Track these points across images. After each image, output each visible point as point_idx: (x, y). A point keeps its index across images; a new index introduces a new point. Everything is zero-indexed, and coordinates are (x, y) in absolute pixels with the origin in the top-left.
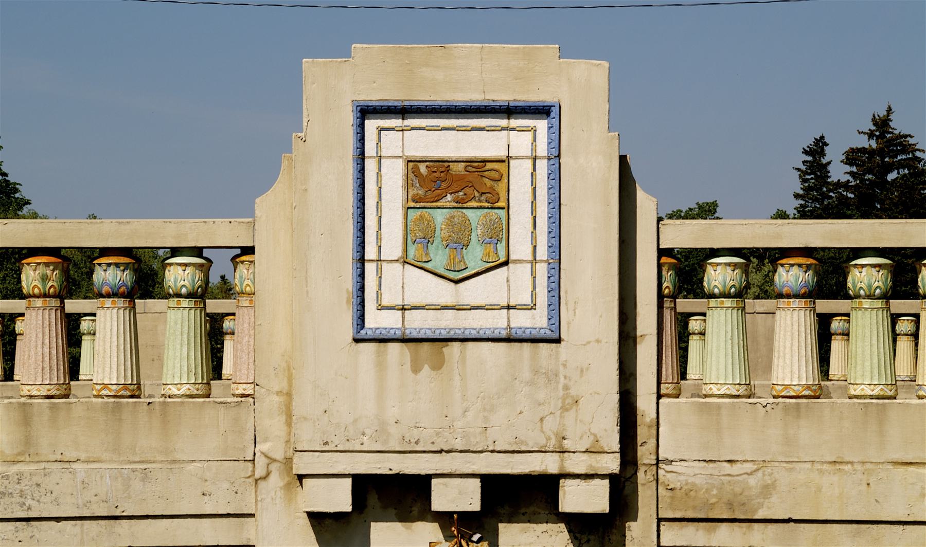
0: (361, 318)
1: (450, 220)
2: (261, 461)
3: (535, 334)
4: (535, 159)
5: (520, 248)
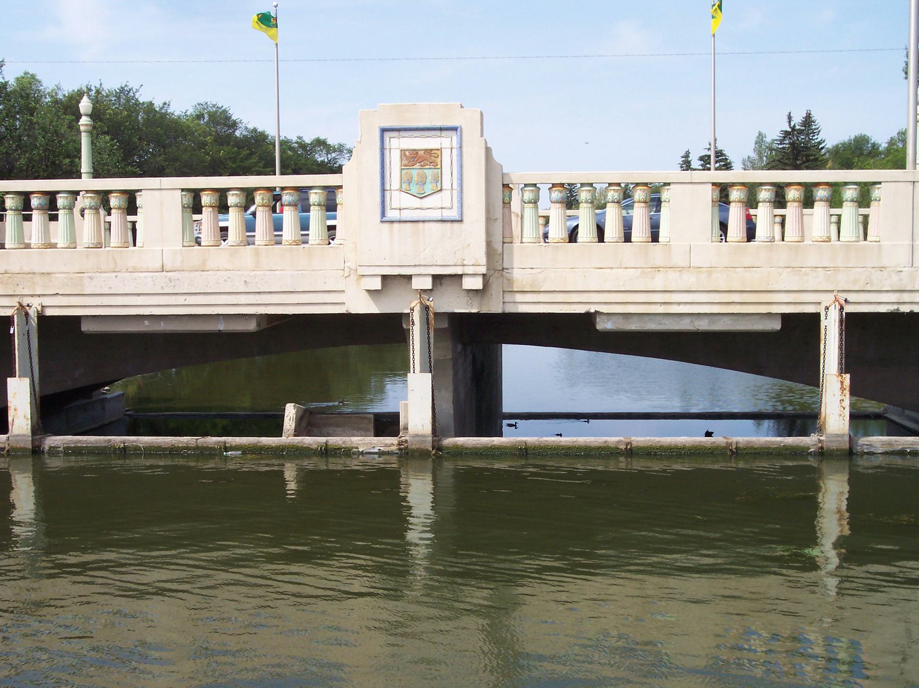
0: (383, 214)
1: (418, 175)
2: (347, 270)
3: (452, 218)
4: (452, 149)
5: (446, 185)
